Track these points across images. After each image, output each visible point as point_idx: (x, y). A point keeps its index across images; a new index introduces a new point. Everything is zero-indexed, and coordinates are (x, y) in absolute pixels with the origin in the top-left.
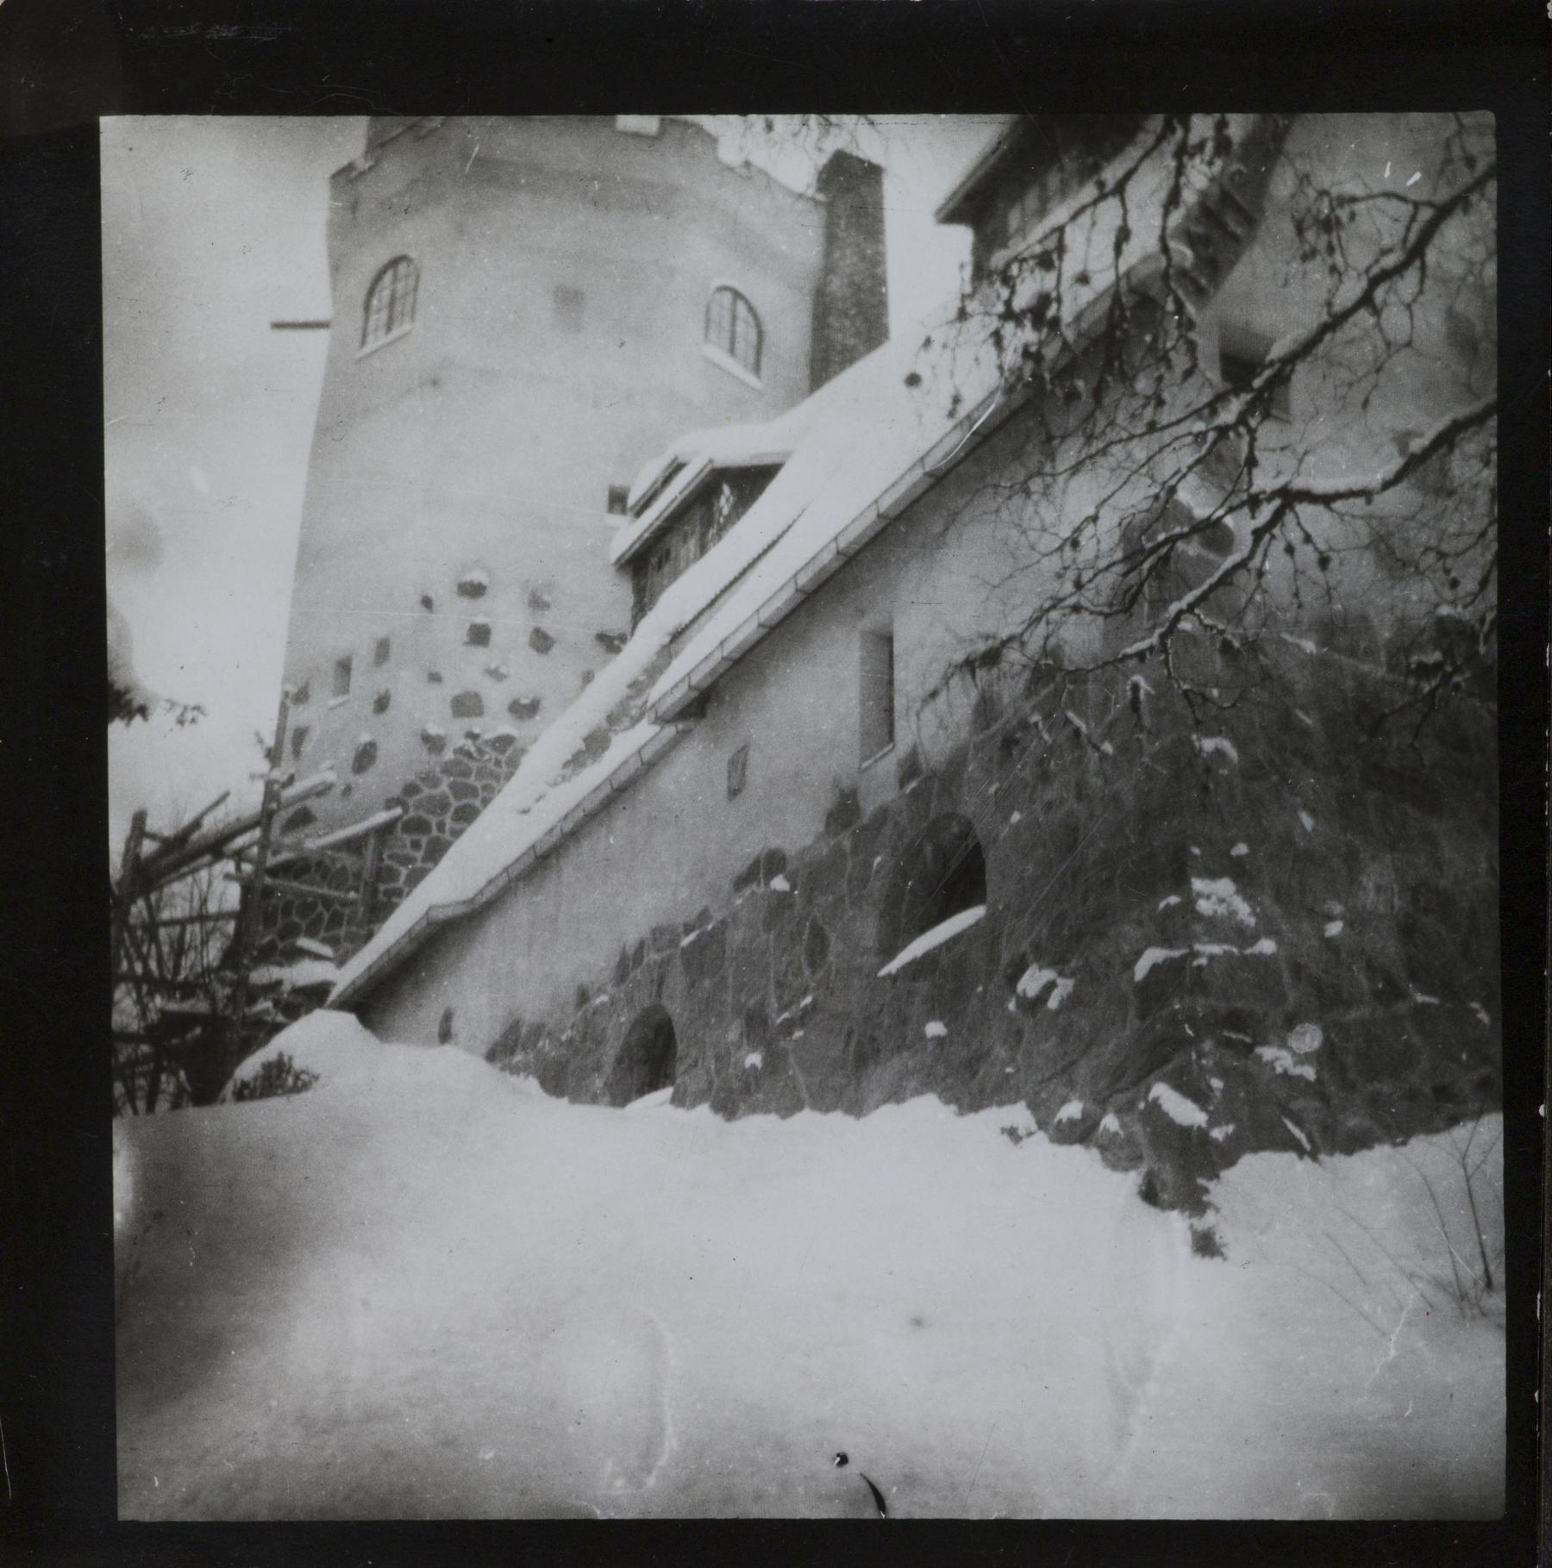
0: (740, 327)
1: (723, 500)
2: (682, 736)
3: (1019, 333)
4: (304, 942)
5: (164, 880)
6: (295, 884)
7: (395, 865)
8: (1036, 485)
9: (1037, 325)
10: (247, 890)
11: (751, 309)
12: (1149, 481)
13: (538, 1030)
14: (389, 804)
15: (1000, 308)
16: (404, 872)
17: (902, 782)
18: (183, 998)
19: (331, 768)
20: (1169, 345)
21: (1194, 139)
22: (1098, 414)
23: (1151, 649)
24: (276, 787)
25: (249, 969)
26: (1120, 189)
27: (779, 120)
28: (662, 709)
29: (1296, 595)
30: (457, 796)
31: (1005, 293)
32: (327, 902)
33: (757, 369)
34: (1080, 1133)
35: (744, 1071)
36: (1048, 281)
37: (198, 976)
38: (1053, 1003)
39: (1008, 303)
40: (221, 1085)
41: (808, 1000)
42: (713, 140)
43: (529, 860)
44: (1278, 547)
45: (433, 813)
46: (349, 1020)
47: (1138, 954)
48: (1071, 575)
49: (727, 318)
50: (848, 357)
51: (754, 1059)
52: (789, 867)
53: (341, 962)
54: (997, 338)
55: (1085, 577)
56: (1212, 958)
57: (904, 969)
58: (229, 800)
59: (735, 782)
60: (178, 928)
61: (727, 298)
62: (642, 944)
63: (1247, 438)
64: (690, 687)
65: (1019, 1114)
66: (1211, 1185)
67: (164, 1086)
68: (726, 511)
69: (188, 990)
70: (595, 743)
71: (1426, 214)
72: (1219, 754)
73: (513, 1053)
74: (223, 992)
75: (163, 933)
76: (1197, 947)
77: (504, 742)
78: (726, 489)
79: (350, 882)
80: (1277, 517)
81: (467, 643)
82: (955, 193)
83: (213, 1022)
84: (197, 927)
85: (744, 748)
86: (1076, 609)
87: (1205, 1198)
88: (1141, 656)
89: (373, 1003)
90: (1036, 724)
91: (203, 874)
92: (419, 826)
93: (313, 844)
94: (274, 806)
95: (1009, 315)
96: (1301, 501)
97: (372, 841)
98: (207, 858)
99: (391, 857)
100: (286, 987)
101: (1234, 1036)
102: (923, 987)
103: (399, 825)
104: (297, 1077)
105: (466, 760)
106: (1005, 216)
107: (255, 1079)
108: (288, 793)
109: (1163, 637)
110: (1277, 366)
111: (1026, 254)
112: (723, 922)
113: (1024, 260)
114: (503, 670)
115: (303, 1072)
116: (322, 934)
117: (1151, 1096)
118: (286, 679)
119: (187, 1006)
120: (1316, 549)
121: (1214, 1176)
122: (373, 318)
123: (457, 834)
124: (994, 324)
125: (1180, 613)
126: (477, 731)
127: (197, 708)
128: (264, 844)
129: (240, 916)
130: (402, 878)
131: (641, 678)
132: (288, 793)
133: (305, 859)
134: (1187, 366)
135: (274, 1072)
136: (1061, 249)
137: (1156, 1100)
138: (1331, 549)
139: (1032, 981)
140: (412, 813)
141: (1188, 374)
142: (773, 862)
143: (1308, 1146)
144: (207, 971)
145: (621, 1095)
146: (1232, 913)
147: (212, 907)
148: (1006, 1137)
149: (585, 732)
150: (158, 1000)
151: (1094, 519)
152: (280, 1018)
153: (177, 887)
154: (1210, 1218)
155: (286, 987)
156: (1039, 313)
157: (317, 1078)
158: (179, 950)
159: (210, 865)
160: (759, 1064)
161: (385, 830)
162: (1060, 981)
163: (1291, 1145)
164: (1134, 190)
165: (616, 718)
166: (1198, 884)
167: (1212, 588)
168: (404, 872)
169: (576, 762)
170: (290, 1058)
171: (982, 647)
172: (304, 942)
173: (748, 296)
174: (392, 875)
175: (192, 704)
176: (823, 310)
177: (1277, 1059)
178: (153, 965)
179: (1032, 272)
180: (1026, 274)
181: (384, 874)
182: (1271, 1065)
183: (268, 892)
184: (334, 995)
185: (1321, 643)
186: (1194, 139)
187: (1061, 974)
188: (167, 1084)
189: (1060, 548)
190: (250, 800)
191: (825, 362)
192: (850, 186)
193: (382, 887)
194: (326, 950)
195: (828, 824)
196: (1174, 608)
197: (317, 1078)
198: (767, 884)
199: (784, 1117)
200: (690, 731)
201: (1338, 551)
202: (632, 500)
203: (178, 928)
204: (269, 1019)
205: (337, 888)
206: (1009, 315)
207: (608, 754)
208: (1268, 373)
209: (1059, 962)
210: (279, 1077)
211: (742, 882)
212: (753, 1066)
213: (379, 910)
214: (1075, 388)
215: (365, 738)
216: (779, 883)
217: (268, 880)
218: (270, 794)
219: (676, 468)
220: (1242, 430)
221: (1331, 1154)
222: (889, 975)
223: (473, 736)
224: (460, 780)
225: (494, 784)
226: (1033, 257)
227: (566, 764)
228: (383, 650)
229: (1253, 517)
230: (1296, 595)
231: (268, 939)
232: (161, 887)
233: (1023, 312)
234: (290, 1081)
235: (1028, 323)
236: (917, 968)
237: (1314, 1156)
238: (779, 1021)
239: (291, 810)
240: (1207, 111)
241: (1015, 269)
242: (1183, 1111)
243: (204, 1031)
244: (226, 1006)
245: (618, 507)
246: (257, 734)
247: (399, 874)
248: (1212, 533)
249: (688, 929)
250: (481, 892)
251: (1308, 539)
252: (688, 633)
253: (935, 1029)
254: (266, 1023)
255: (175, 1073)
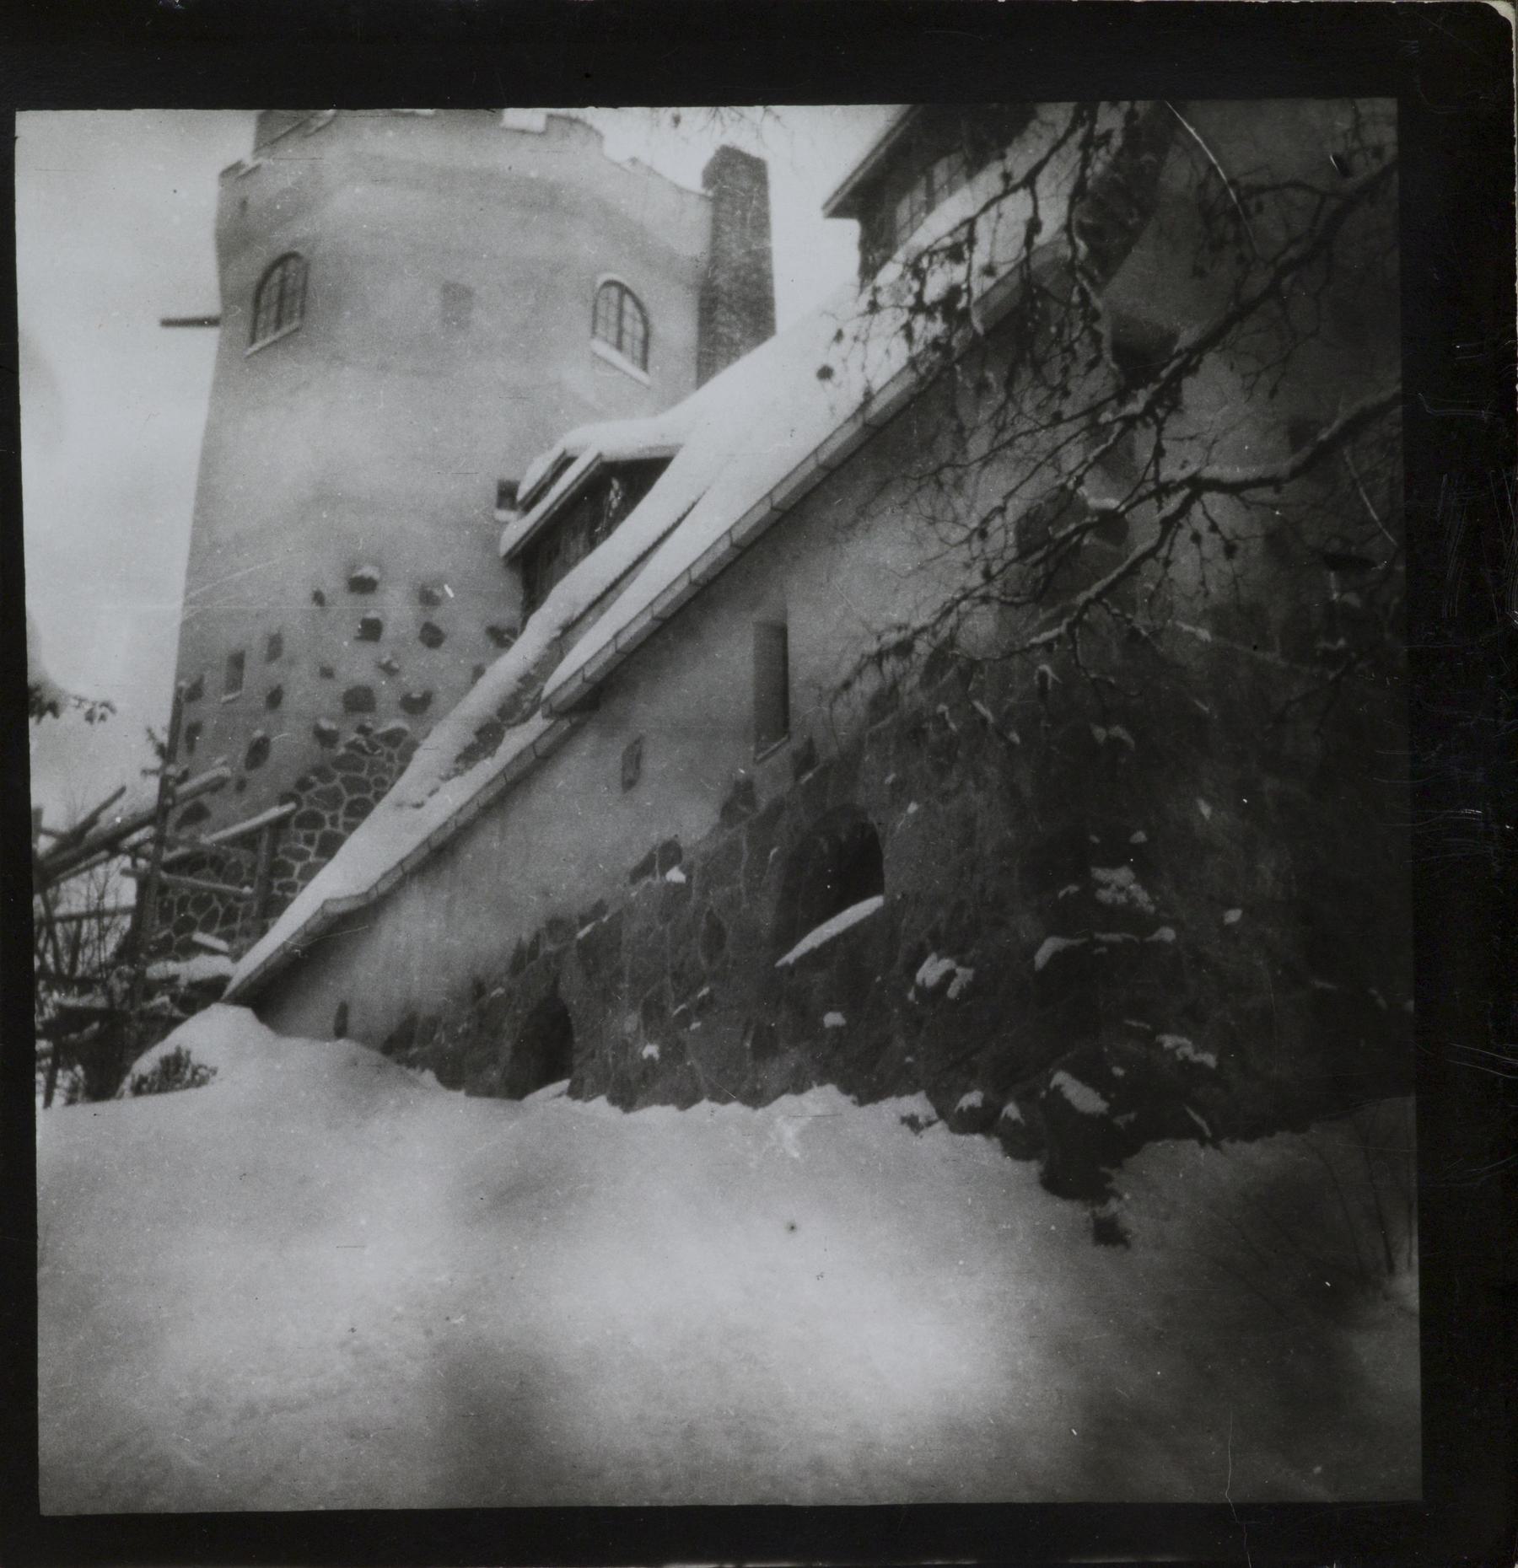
0: (628, 323)
1: (612, 494)
2: (575, 731)
3: (930, 325)
4: (199, 937)
5: (61, 876)
6: (190, 880)
7: (290, 861)
8: (948, 476)
9: (947, 318)
10: (143, 887)
11: (639, 305)
12: (1055, 473)
13: (434, 1022)
14: (283, 800)
15: (910, 300)
16: (298, 866)
17: (798, 775)
18: (81, 994)
19: (225, 764)
20: (1075, 335)
21: (1100, 128)
22: (1010, 405)
23: (1059, 638)
24: (171, 783)
25: (147, 964)
26: (1029, 181)
27: (686, 112)
28: (555, 703)
29: (1203, 583)
30: (350, 790)
31: (916, 286)
32: (222, 896)
33: (644, 364)
34: (966, 1123)
35: (643, 1061)
36: (958, 273)
37: (94, 972)
38: (952, 992)
39: (919, 296)
40: (120, 1080)
41: (705, 991)
42: (599, 136)
43: (425, 852)
44: (1184, 536)
45: (326, 808)
46: (245, 1014)
47: (1040, 943)
48: (979, 566)
49: (614, 312)
50: (733, 352)
51: (651, 1050)
52: (685, 858)
53: (236, 956)
54: (908, 330)
55: (995, 569)
56: (1112, 946)
57: (802, 961)
58: (125, 797)
59: (630, 774)
60: (74, 924)
61: (614, 292)
62: (537, 936)
63: (1155, 428)
64: (584, 680)
65: (917, 1104)
66: (1114, 1173)
67: (59, 1082)
68: (615, 504)
69: (86, 985)
70: (487, 736)
71: (1333, 204)
72: (1114, 743)
73: (408, 1046)
74: (119, 986)
75: (58, 927)
76: (1097, 935)
77: (393, 738)
78: (616, 484)
79: (245, 877)
80: (1184, 510)
81: (357, 638)
82: (843, 186)
83: (109, 1016)
84: (94, 922)
85: (637, 742)
86: (985, 599)
87: (1108, 1186)
88: (1048, 645)
89: (269, 997)
90: (943, 714)
91: (100, 870)
92: (313, 820)
93: (207, 839)
94: (169, 801)
95: (919, 307)
96: (1209, 490)
97: (266, 835)
98: (104, 854)
99: (285, 852)
100: (183, 982)
101: (1134, 1024)
102: (819, 978)
103: (294, 819)
104: (195, 1072)
105: (357, 754)
106: (893, 212)
107: (154, 1073)
108: (185, 788)
109: (1070, 627)
110: (1185, 356)
111: (936, 247)
112: (619, 913)
113: (935, 252)
114: (395, 665)
115: (200, 1066)
116: (217, 930)
117: (1052, 1085)
118: (180, 676)
119: (83, 1002)
120: (1223, 538)
121: (1118, 1164)
122: (263, 316)
123: (351, 828)
124: (904, 317)
125: (1089, 602)
126: (369, 725)
127: (106, 705)
128: (159, 841)
129: (138, 912)
130: (297, 871)
131: (533, 672)
132: (185, 788)
133: (200, 854)
134: (1092, 356)
135: (172, 1068)
136: (971, 241)
137: (1058, 1088)
138: (1237, 537)
139: (931, 971)
140: (305, 809)
141: (1092, 365)
142: (670, 853)
143: (1208, 1133)
144: (103, 967)
145: (516, 1089)
146: (1132, 901)
147: (109, 903)
148: (906, 1128)
149: (476, 725)
150: (56, 995)
151: (1002, 510)
152: (177, 1013)
153: (73, 883)
154: (1114, 1206)
155: (183, 982)
156: (949, 305)
157: (214, 1072)
158: (75, 945)
159: (107, 860)
160: (657, 1056)
161: (280, 824)
162: (959, 970)
163: (1193, 1132)
164: (1043, 182)
165: (511, 711)
166: (1100, 874)
167: (1121, 577)
168: (298, 866)
169: (469, 756)
170: (188, 1053)
171: (893, 637)
172: (199, 937)
173: (636, 292)
174: (288, 871)
175: (100, 698)
176: (709, 304)
177: (1178, 1047)
178: (49, 959)
179: (942, 264)
180: (935, 267)
181: (278, 869)
182: (1172, 1051)
183: (163, 889)
184: (232, 986)
185: (1216, 632)
186: (1100, 128)
187: (961, 963)
188: (63, 1079)
189: (968, 540)
190: (147, 793)
191: (712, 354)
192: (737, 180)
193: (276, 882)
194: (221, 945)
195: (722, 815)
196: (1081, 598)
197: (214, 1072)
198: (663, 873)
199: (862, 1101)
200: (584, 725)
201: (1244, 540)
202: (520, 497)
203: (74, 924)
204: (165, 1013)
205: (231, 883)
206: (919, 307)
207: (501, 749)
208: (1175, 363)
209: (957, 952)
210: (177, 1071)
211: (643, 870)
212: (651, 1057)
213: (273, 907)
214: (986, 379)
215: (259, 733)
216: (676, 875)
217: (164, 875)
218: (165, 790)
219: (565, 462)
220: (1150, 420)
221: (1232, 1141)
222: (787, 965)
223: (362, 730)
224: (353, 774)
225: (387, 778)
226: (943, 250)
227: (458, 759)
228: (275, 647)
229: (1160, 508)
230: (1203, 583)
231: (162, 935)
232: (58, 884)
233: (935, 305)
234: (188, 1075)
235: (938, 315)
236: (815, 958)
237: (1215, 1142)
238: (676, 1012)
239: (187, 805)
240: (1114, 101)
241: (925, 263)
242: (1084, 1098)
243: (101, 1024)
244: (123, 1002)
245: (507, 501)
246: (149, 731)
247: (293, 868)
248: (1112, 524)
249: (584, 921)
250: (376, 886)
251: (1214, 528)
252: (578, 627)
253: (833, 1019)
254: (162, 1018)
255: (71, 1068)
